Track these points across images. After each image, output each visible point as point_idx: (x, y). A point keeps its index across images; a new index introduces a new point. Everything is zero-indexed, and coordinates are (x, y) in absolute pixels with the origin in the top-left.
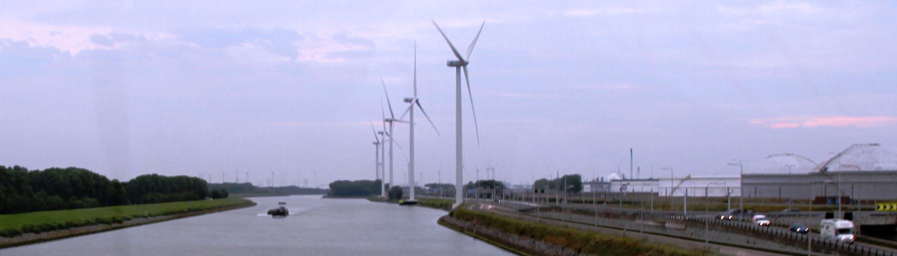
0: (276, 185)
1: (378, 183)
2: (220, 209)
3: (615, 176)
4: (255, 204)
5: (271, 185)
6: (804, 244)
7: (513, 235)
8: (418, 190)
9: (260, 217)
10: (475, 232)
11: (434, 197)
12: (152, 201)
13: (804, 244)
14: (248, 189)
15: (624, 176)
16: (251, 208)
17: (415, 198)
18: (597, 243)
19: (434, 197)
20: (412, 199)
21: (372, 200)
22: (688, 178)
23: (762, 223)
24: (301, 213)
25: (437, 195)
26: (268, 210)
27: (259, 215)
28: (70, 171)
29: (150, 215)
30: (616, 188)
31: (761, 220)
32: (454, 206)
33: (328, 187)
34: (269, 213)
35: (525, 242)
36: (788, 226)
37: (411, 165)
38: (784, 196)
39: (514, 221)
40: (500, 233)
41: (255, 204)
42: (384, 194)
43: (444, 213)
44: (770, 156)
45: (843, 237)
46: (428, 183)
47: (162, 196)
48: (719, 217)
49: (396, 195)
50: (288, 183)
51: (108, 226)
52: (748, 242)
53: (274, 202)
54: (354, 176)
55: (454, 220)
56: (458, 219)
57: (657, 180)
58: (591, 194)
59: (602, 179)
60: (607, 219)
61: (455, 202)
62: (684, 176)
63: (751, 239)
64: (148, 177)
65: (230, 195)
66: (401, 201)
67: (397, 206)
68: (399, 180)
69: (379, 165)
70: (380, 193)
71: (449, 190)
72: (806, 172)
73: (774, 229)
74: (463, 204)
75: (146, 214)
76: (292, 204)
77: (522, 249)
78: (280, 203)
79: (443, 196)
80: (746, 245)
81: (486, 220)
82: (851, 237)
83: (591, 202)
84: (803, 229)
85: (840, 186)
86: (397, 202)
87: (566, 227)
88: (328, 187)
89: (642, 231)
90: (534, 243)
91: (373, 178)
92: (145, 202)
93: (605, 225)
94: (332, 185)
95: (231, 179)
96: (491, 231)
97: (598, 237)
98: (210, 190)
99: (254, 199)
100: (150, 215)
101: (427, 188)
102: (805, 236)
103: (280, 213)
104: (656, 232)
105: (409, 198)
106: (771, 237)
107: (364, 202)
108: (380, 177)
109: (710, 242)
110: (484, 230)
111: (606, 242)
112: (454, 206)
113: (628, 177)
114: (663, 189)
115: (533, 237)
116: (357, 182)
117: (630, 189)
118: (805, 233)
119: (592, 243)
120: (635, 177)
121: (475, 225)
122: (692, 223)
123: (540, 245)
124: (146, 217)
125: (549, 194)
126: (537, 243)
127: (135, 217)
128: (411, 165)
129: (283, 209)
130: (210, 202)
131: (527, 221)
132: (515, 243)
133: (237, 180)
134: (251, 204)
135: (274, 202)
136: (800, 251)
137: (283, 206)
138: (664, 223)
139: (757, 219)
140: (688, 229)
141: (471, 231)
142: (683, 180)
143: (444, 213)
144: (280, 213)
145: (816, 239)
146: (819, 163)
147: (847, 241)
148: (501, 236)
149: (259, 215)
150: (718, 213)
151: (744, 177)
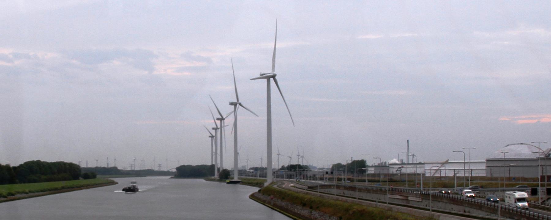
0: (137, 168)
1: (213, 167)
2: (87, 187)
3: (395, 161)
4: (117, 183)
5: (133, 169)
6: (494, 210)
7: (298, 207)
8: (242, 172)
9: (116, 192)
10: (272, 204)
11: (253, 178)
12: (35, 181)
13: (494, 210)
14: (114, 172)
15: (402, 160)
16: (117, 185)
17: (238, 178)
18: (354, 212)
19: (253, 178)
20: (236, 179)
21: (207, 180)
22: (447, 162)
23: (469, 195)
24: (149, 190)
25: (255, 176)
26: (122, 189)
27: (115, 192)
28: (26, 164)
29: (30, 192)
30: (393, 170)
31: (468, 193)
32: (266, 184)
33: (175, 170)
34: (123, 190)
35: (305, 212)
36: (485, 197)
37: (236, 153)
38: (495, 175)
39: (301, 195)
40: (290, 205)
41: (117, 183)
42: (216, 176)
43: (256, 189)
44: (508, 145)
45: (520, 204)
46: (252, 167)
47: (43, 177)
48: (441, 192)
49: (225, 176)
50: (147, 167)
51: (5, 199)
52: (426, 206)
53: (126, 182)
54: (195, 162)
55: (261, 196)
56: (263, 194)
57: (424, 164)
58: (373, 175)
59: (385, 163)
60: (368, 194)
61: (266, 181)
62: (444, 161)
63: (467, 209)
64: (33, 162)
65: (98, 176)
66: (228, 181)
67: (225, 184)
68: (228, 165)
69: (214, 154)
70: (214, 175)
71: (260, 171)
72: (534, 156)
73: (476, 200)
74: (273, 183)
75: (27, 190)
76: (143, 184)
77: (295, 214)
78: (132, 183)
79: (260, 177)
80: (425, 207)
81: (283, 195)
82: (526, 204)
83: (364, 181)
84: (495, 199)
85: (455, 173)
86: (225, 182)
87: (337, 200)
88: (175, 170)
89: (387, 202)
90: (311, 212)
91: (209, 163)
92: (30, 181)
93: (367, 198)
94: (179, 169)
95: (103, 164)
96: (284, 204)
97: (355, 207)
98: (83, 172)
99: (115, 180)
100: (30, 192)
101: (252, 171)
102: (496, 204)
103: (132, 190)
104: (397, 203)
105: (233, 178)
106: (480, 207)
107: (202, 181)
108: (214, 163)
109: (433, 211)
110: (279, 202)
111: (360, 211)
112: (266, 184)
113: (405, 161)
114: (429, 171)
115: (311, 208)
116: (198, 166)
117: (404, 171)
118: (497, 202)
119: (351, 212)
120: (410, 162)
121: (272, 199)
122: (426, 196)
123: (316, 214)
124: (27, 193)
125: (347, 175)
126: (314, 212)
127: (18, 193)
128: (236, 153)
129: (134, 187)
130: (82, 181)
131: (314, 195)
132: (298, 212)
133: (108, 164)
134: (113, 183)
135: (126, 182)
136: (492, 216)
137: (134, 184)
138: (408, 197)
139: (466, 192)
140: (424, 201)
141: (269, 203)
142: (443, 164)
143: (256, 189)
144: (132, 190)
145: (503, 206)
146: (544, 150)
147: (524, 208)
148: (290, 207)
149: (115, 192)
150: (440, 189)
151: (488, 161)
